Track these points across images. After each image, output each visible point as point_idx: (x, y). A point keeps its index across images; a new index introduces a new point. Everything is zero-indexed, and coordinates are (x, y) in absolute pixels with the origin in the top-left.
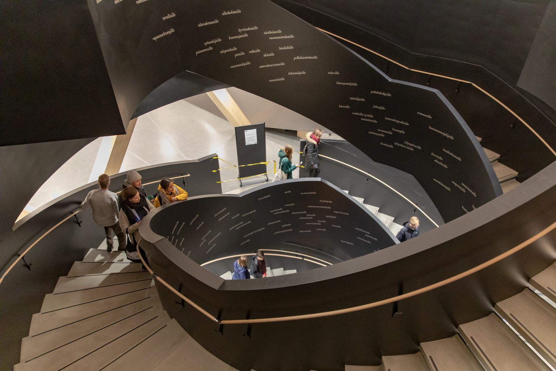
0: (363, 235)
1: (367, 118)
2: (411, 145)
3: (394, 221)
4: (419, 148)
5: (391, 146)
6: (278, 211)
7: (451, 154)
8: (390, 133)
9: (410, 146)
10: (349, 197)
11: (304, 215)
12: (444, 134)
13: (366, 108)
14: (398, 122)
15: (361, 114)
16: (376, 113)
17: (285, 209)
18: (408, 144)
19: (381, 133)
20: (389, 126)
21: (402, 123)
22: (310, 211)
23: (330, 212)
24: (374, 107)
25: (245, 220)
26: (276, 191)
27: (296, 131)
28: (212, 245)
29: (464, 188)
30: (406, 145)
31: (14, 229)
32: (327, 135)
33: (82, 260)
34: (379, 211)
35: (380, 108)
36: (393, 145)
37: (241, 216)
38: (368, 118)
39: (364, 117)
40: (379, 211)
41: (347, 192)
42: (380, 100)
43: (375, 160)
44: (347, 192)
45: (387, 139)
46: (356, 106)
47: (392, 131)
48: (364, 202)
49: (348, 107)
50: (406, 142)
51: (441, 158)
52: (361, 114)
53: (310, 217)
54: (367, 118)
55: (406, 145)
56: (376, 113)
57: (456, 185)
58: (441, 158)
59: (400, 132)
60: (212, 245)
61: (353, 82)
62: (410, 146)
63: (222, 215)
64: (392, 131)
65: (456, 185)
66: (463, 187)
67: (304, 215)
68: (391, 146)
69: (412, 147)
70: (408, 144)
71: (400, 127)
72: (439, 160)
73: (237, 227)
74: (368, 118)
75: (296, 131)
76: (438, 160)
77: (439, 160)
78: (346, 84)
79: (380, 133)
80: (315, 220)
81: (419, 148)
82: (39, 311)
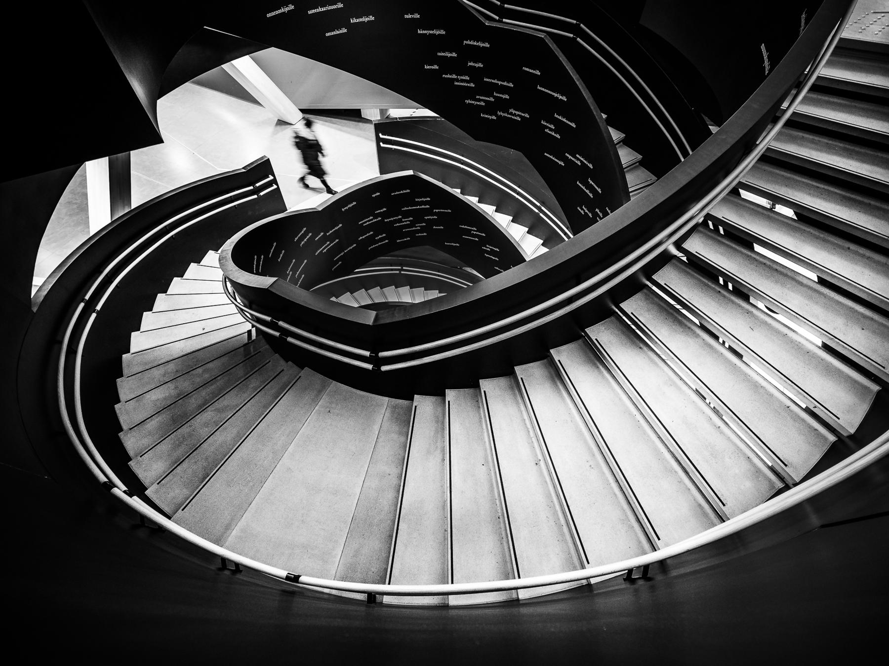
0: (468, 233)
1: (462, 81)
2: (517, 113)
3: (512, 221)
4: (527, 116)
5: (494, 118)
6: (367, 222)
7: (564, 120)
8: (492, 99)
9: (516, 115)
10: (461, 197)
11: (400, 221)
12: (556, 95)
13: (457, 66)
14: (500, 83)
15: (454, 76)
16: (471, 72)
17: (376, 216)
18: (514, 112)
19: (481, 101)
20: (489, 89)
21: (505, 84)
22: (406, 214)
23: (430, 212)
24: (469, 64)
25: (331, 239)
26: (363, 197)
27: (359, 110)
28: (300, 276)
29: (579, 160)
30: (511, 114)
31: (35, 309)
32: (404, 110)
33: (151, 310)
34: (496, 211)
35: (477, 65)
36: (496, 115)
37: (325, 234)
38: (463, 81)
39: (457, 80)
40: (496, 211)
41: (459, 191)
42: (476, 54)
43: (477, 138)
44: (459, 191)
45: (490, 108)
46: (447, 65)
47: (494, 97)
48: (479, 202)
49: (436, 67)
50: (511, 110)
51: (552, 127)
52: (454, 76)
53: (407, 221)
54: (462, 81)
55: (511, 114)
56: (475, 75)
57: (570, 157)
58: (552, 127)
59: (504, 97)
60: (300, 276)
61: (438, 28)
62: (516, 115)
63: (303, 236)
64: (494, 97)
65: (570, 157)
66: (578, 159)
67: (400, 221)
68: (494, 118)
69: (519, 115)
70: (514, 112)
71: (503, 89)
72: (551, 129)
73: (324, 249)
74: (463, 81)
75: (359, 110)
76: (550, 129)
77: (551, 129)
78: (431, 32)
79: (480, 100)
80: (412, 224)
81: (527, 116)
82: (151, 310)
